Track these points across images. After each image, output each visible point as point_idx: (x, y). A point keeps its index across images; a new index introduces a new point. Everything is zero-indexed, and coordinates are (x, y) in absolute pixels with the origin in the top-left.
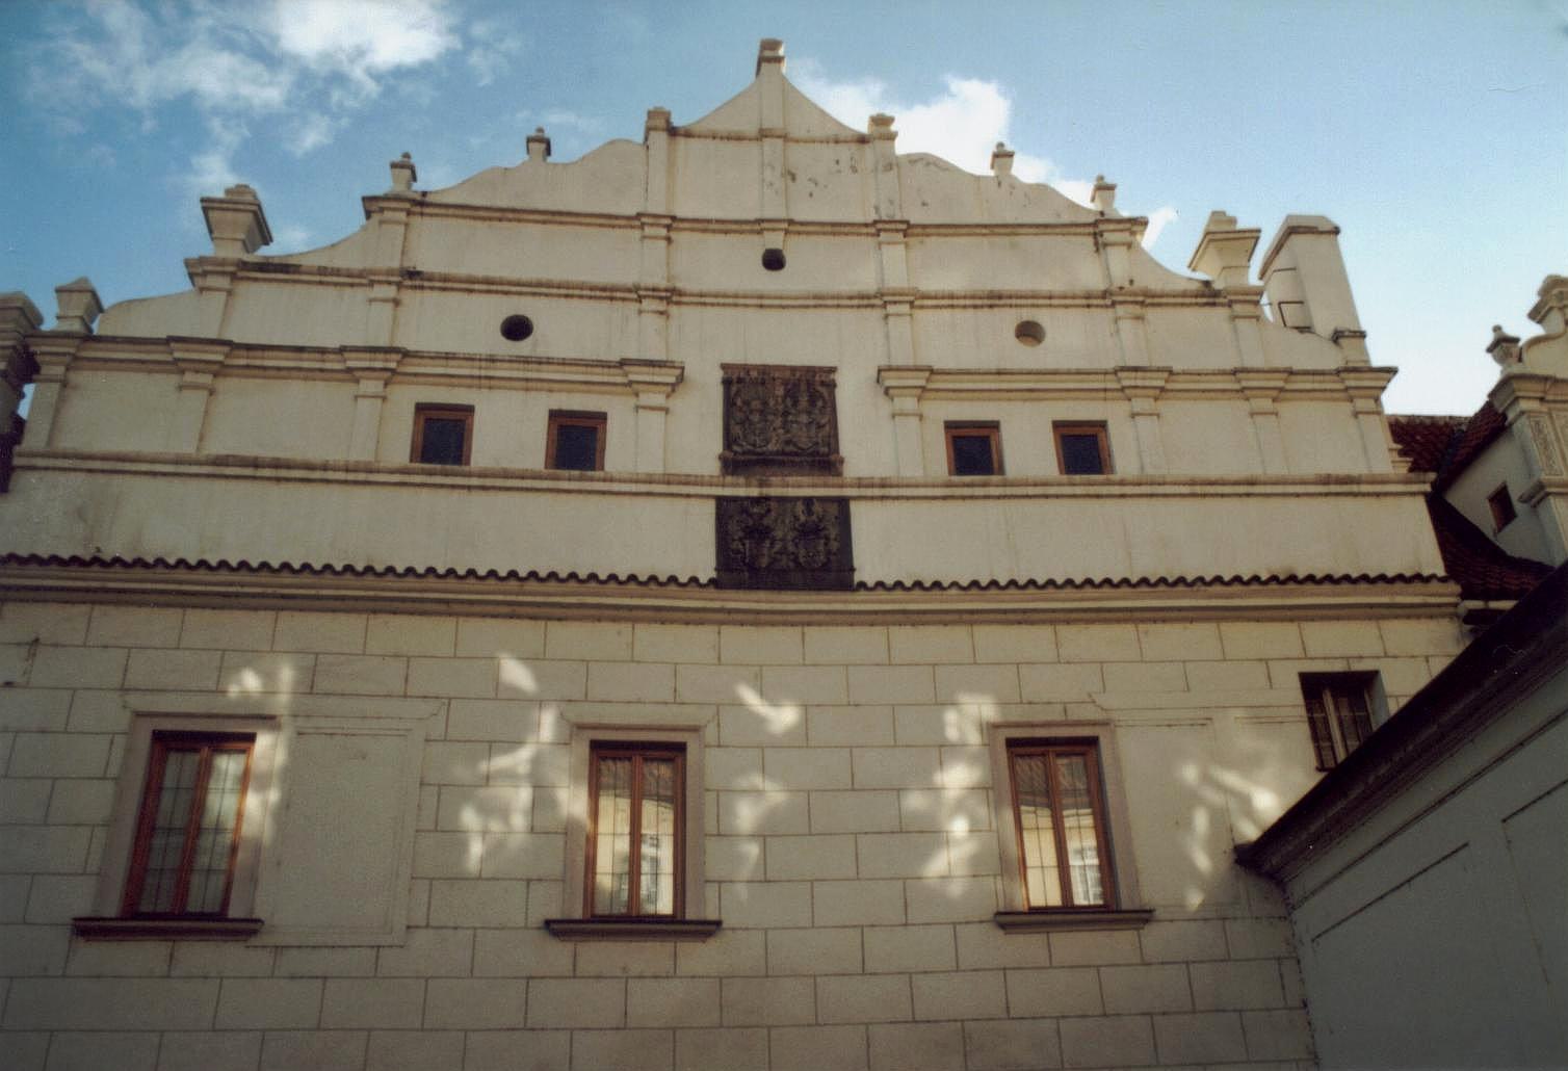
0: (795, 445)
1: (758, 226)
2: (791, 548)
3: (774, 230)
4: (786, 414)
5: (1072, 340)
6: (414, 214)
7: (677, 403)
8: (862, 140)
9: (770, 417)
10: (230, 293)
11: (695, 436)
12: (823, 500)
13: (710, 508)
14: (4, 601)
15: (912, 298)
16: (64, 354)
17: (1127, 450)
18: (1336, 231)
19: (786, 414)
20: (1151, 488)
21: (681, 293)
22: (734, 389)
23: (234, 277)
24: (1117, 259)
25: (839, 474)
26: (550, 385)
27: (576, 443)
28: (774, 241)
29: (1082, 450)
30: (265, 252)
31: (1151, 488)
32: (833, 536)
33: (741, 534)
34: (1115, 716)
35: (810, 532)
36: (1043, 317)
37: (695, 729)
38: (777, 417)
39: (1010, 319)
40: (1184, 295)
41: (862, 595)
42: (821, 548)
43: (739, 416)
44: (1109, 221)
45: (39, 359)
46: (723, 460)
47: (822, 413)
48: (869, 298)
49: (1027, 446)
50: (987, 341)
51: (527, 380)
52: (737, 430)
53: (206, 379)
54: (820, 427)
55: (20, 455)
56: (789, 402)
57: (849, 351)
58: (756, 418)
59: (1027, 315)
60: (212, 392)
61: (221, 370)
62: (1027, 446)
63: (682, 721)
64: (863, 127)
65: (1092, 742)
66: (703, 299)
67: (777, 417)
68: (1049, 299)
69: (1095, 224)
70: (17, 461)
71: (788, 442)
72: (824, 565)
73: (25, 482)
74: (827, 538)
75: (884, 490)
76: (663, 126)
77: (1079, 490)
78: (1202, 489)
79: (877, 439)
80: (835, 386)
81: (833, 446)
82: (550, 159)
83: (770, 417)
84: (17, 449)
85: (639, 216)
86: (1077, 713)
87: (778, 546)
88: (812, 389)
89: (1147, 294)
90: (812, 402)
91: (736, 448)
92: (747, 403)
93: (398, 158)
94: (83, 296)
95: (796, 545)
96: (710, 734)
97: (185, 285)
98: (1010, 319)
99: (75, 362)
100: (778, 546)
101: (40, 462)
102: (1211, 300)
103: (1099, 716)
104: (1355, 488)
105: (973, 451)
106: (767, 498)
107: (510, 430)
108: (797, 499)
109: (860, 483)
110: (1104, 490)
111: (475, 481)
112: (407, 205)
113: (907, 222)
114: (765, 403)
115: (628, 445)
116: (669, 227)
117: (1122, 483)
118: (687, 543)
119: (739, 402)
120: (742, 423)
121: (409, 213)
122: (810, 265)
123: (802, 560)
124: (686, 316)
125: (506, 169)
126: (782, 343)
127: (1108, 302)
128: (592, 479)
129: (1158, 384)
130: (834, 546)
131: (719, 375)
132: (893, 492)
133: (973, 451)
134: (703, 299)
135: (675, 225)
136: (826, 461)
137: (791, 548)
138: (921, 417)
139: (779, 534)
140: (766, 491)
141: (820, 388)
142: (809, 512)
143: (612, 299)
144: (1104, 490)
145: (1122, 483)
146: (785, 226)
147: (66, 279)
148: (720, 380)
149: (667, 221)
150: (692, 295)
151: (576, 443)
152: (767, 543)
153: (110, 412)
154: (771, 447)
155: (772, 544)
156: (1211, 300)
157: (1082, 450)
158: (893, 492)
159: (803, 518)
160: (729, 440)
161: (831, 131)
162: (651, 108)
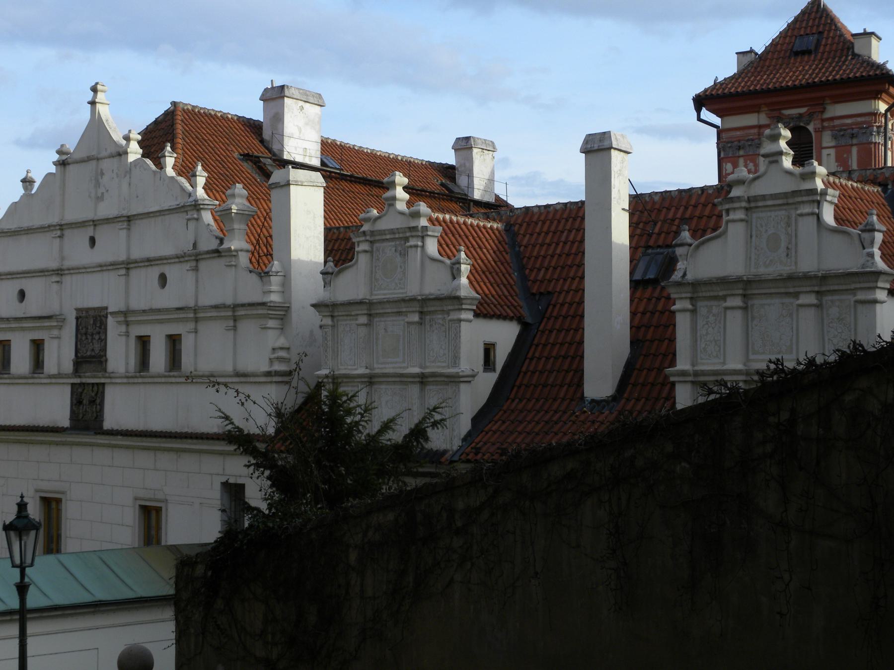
5: (182, 287)
11: (61, 353)
13: (68, 390)
25: (105, 370)
37: (63, 493)
39: (154, 273)
71: (93, 350)
72: (96, 418)
103: (160, 496)
106: (84, 384)
116: (61, 230)
118: (53, 406)
131: (74, 314)
140: (84, 380)
154: (89, 353)
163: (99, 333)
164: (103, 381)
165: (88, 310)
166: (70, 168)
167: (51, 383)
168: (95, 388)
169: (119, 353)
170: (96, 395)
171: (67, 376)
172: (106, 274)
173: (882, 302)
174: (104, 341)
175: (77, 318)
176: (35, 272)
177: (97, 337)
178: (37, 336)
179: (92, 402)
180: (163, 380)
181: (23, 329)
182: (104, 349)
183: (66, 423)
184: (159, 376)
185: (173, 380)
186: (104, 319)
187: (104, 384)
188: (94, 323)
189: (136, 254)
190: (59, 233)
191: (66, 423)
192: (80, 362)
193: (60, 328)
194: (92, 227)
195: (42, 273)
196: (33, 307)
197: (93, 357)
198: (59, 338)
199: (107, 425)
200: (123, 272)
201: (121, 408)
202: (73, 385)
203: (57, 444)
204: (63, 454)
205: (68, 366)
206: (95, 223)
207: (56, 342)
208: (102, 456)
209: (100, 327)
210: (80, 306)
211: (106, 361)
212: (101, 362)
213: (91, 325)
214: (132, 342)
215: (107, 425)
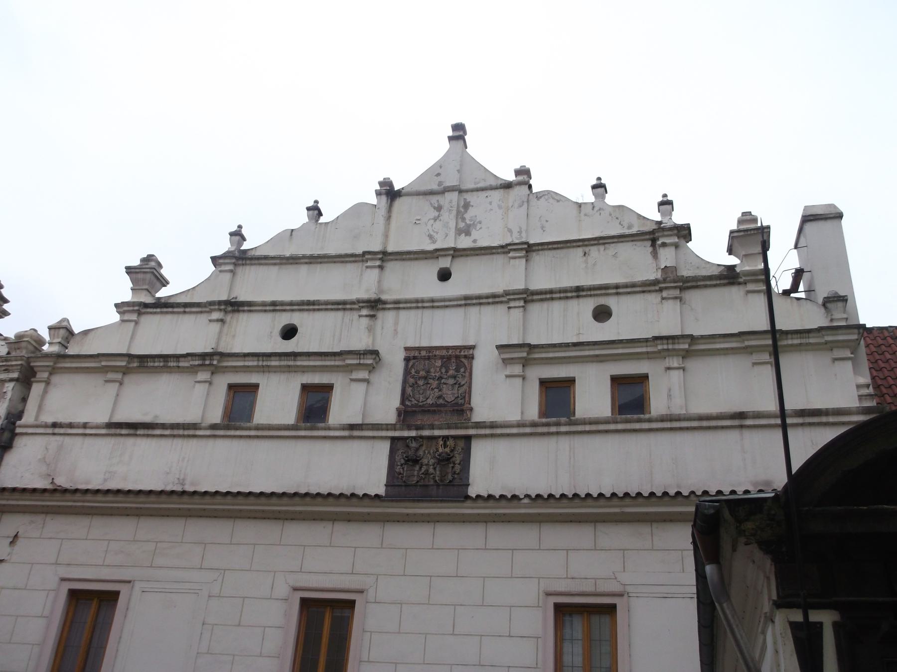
0: (444, 399)
1: (435, 254)
2: (431, 470)
3: (445, 255)
4: (440, 378)
5: (634, 319)
6: (239, 265)
7: (375, 378)
8: (508, 186)
9: (431, 381)
10: (136, 323)
11: (374, 399)
12: (455, 437)
13: (386, 446)
14: (3, 512)
15: (525, 296)
16: (47, 366)
17: (666, 392)
18: (839, 216)
19: (440, 378)
20: (675, 423)
21: (385, 303)
22: (411, 363)
23: (140, 314)
24: (667, 257)
26: (304, 370)
27: (314, 407)
28: (445, 263)
29: (630, 398)
30: (163, 293)
31: (675, 423)
32: (458, 462)
33: (403, 461)
34: (629, 589)
35: (445, 460)
36: (612, 302)
37: (361, 592)
38: (437, 378)
39: (588, 305)
40: (710, 278)
41: (469, 503)
42: (450, 470)
43: (412, 381)
44: (664, 229)
45: (36, 369)
46: (399, 412)
47: (463, 377)
48: (498, 296)
49: (593, 397)
50: (571, 323)
51: (528, 297)
52: (409, 390)
53: (119, 376)
54: (460, 386)
55: (20, 426)
56: (443, 370)
57: (485, 332)
58: (421, 383)
59: (602, 301)
60: (121, 384)
61: (126, 371)
62: (593, 397)
63: (354, 586)
64: (511, 177)
65: (611, 609)
66: (399, 305)
67: (437, 378)
68: (617, 289)
69: (653, 232)
70: (18, 430)
71: (439, 397)
72: (450, 481)
73: (19, 442)
74: (454, 464)
75: (495, 430)
76: (389, 192)
77: (620, 426)
78: (707, 423)
79: (499, 395)
80: (473, 358)
81: (467, 399)
82: (322, 220)
83: (431, 381)
84: (18, 423)
85: (365, 253)
86: (603, 587)
87: (423, 470)
88: (459, 359)
89: (687, 280)
90: (457, 370)
91: (407, 403)
92: (417, 372)
93: (595, 182)
94: (63, 330)
95: (435, 469)
96: (371, 595)
97: (116, 318)
98: (588, 305)
99: (53, 371)
100: (423, 470)
101: (30, 430)
102: (731, 281)
104: (824, 419)
105: (557, 396)
106: (422, 437)
107: (278, 401)
108: (439, 437)
109: (479, 425)
110: (637, 426)
111: (253, 433)
112: (234, 261)
113: (527, 243)
114: (428, 372)
115: (345, 407)
116: (382, 260)
118: (365, 469)
119: (413, 371)
120: (412, 386)
121: (235, 265)
122: (471, 278)
123: (437, 478)
124: (387, 318)
125: (292, 230)
126: (444, 331)
127: (657, 288)
128: (318, 429)
129: (685, 348)
130: (458, 468)
131: (402, 355)
132: (499, 431)
133: (557, 396)
134: (399, 305)
135: (386, 258)
136: (461, 408)
137: (431, 470)
138: (524, 378)
139: (425, 461)
141: (463, 360)
142: (445, 446)
143: (344, 309)
144: (637, 426)
146: (452, 252)
147: (53, 321)
148: (403, 357)
149: (380, 256)
150: (390, 303)
151: (314, 407)
152: (417, 468)
153: (66, 399)
154: (430, 401)
155: (421, 468)
156: (731, 281)
157: (630, 398)
158: (499, 431)
159: (441, 450)
160: (404, 397)
161: (493, 183)
162: (518, 167)
163: (455, 377)
164: (471, 432)
167: (802, 425)
168: (450, 443)
170: (452, 451)
172: (473, 311)
173: (655, 255)
175: (407, 360)
176: (327, 303)
181: (289, 369)
186: (465, 361)
187: (468, 439)
189: (535, 286)
190: (378, 263)
191: (381, 491)
193: (371, 369)
194: (450, 258)
197: (441, 405)
198: (367, 381)
199: (472, 492)
200: (522, 303)
201: (493, 468)
202: (393, 439)
204: (369, 534)
205: (391, 417)
206: (457, 253)
207: (362, 387)
208: (471, 535)
209: (457, 370)
210: (411, 344)
215: (472, 492)
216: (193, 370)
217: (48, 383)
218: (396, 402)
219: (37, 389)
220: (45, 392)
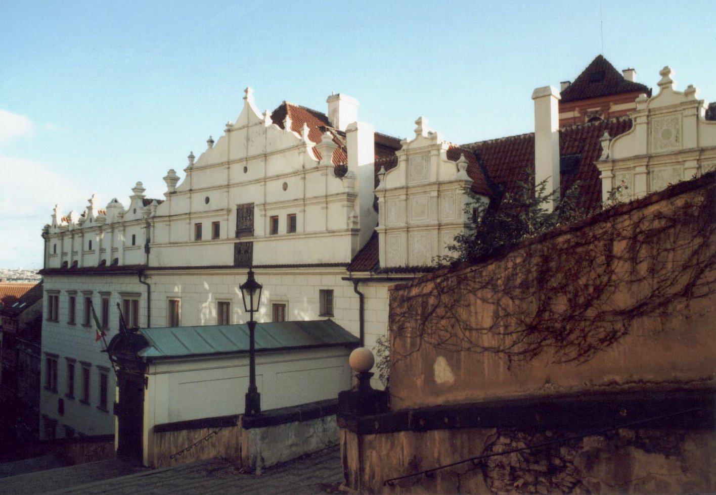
11: (229, 227)
25: (253, 235)
34: (289, 299)
37: (231, 299)
117: (281, 237)
144: (295, 237)
145: (281, 237)
154: (244, 227)
165: (243, 205)
166: (233, 134)
169: (260, 225)
171: (233, 239)
174: (252, 220)
175: (237, 210)
177: (248, 218)
178: (215, 220)
179: (246, 252)
180: (286, 238)
181: (208, 217)
182: (252, 225)
183: (232, 263)
184: (284, 236)
185: (292, 237)
187: (252, 242)
188: (247, 212)
191: (232, 263)
192: (239, 233)
195: (220, 187)
196: (213, 205)
202: (235, 244)
203: (227, 274)
205: (233, 234)
211: (254, 230)
212: (251, 232)
213: (245, 213)
214: (268, 220)
216: (185, 219)
217: (154, 226)
218: (235, 229)
219: (152, 229)
220: (154, 230)
